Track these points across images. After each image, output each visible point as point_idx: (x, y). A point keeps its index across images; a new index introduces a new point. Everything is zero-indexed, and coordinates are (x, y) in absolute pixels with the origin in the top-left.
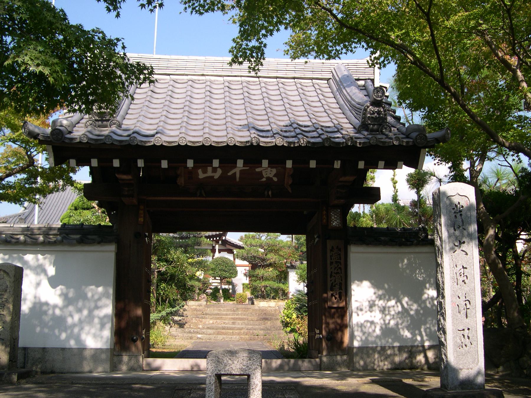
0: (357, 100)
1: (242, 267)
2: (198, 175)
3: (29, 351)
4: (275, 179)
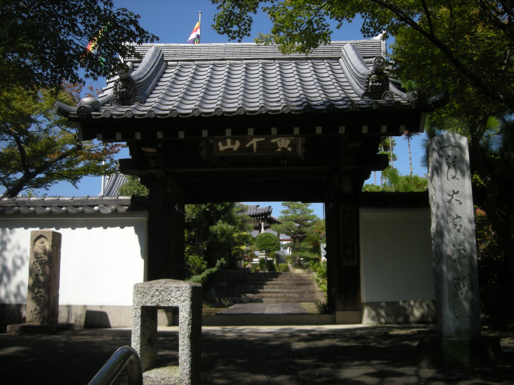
0: (362, 72)
1: (285, 240)
2: (219, 147)
3: (73, 309)
4: (290, 149)
